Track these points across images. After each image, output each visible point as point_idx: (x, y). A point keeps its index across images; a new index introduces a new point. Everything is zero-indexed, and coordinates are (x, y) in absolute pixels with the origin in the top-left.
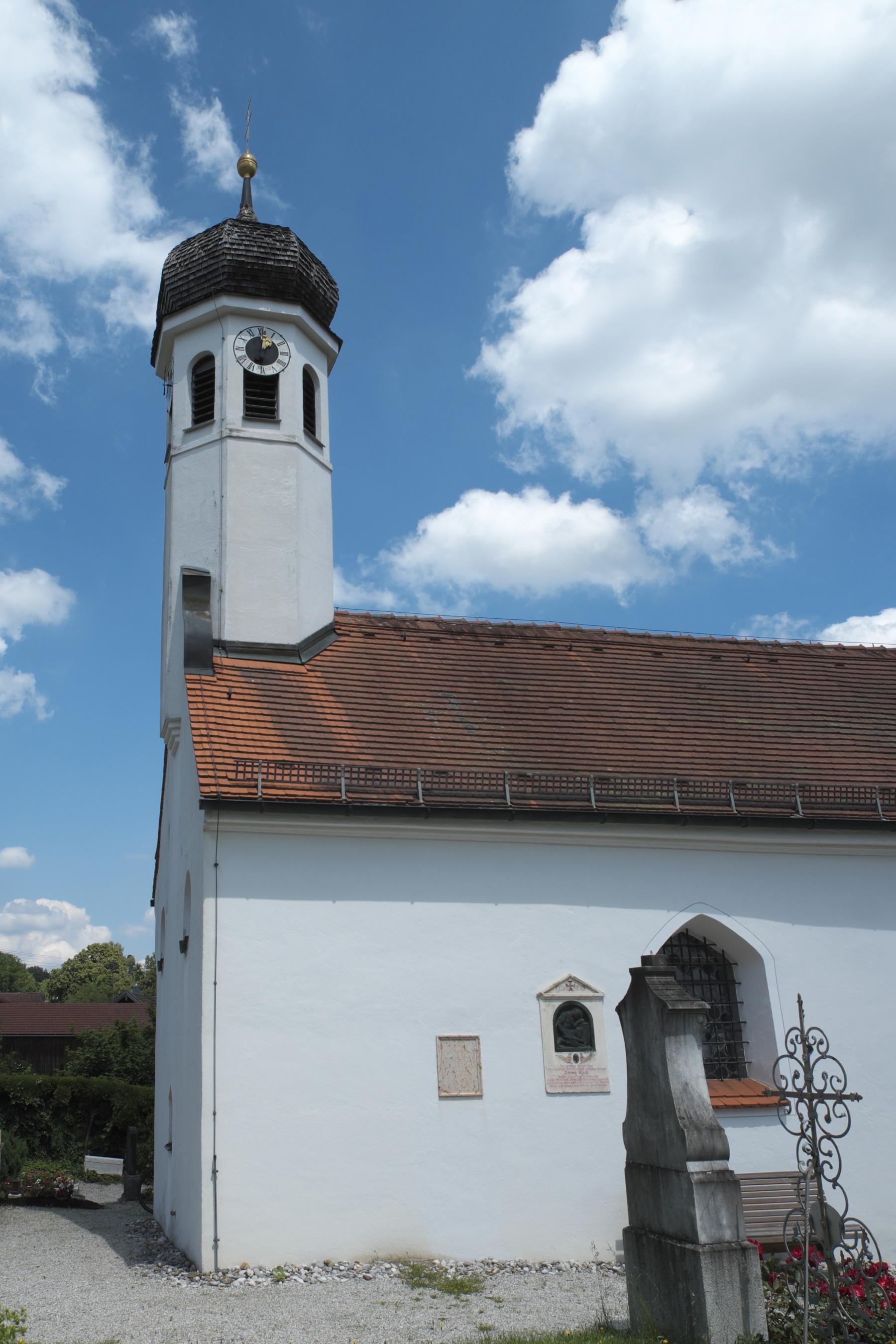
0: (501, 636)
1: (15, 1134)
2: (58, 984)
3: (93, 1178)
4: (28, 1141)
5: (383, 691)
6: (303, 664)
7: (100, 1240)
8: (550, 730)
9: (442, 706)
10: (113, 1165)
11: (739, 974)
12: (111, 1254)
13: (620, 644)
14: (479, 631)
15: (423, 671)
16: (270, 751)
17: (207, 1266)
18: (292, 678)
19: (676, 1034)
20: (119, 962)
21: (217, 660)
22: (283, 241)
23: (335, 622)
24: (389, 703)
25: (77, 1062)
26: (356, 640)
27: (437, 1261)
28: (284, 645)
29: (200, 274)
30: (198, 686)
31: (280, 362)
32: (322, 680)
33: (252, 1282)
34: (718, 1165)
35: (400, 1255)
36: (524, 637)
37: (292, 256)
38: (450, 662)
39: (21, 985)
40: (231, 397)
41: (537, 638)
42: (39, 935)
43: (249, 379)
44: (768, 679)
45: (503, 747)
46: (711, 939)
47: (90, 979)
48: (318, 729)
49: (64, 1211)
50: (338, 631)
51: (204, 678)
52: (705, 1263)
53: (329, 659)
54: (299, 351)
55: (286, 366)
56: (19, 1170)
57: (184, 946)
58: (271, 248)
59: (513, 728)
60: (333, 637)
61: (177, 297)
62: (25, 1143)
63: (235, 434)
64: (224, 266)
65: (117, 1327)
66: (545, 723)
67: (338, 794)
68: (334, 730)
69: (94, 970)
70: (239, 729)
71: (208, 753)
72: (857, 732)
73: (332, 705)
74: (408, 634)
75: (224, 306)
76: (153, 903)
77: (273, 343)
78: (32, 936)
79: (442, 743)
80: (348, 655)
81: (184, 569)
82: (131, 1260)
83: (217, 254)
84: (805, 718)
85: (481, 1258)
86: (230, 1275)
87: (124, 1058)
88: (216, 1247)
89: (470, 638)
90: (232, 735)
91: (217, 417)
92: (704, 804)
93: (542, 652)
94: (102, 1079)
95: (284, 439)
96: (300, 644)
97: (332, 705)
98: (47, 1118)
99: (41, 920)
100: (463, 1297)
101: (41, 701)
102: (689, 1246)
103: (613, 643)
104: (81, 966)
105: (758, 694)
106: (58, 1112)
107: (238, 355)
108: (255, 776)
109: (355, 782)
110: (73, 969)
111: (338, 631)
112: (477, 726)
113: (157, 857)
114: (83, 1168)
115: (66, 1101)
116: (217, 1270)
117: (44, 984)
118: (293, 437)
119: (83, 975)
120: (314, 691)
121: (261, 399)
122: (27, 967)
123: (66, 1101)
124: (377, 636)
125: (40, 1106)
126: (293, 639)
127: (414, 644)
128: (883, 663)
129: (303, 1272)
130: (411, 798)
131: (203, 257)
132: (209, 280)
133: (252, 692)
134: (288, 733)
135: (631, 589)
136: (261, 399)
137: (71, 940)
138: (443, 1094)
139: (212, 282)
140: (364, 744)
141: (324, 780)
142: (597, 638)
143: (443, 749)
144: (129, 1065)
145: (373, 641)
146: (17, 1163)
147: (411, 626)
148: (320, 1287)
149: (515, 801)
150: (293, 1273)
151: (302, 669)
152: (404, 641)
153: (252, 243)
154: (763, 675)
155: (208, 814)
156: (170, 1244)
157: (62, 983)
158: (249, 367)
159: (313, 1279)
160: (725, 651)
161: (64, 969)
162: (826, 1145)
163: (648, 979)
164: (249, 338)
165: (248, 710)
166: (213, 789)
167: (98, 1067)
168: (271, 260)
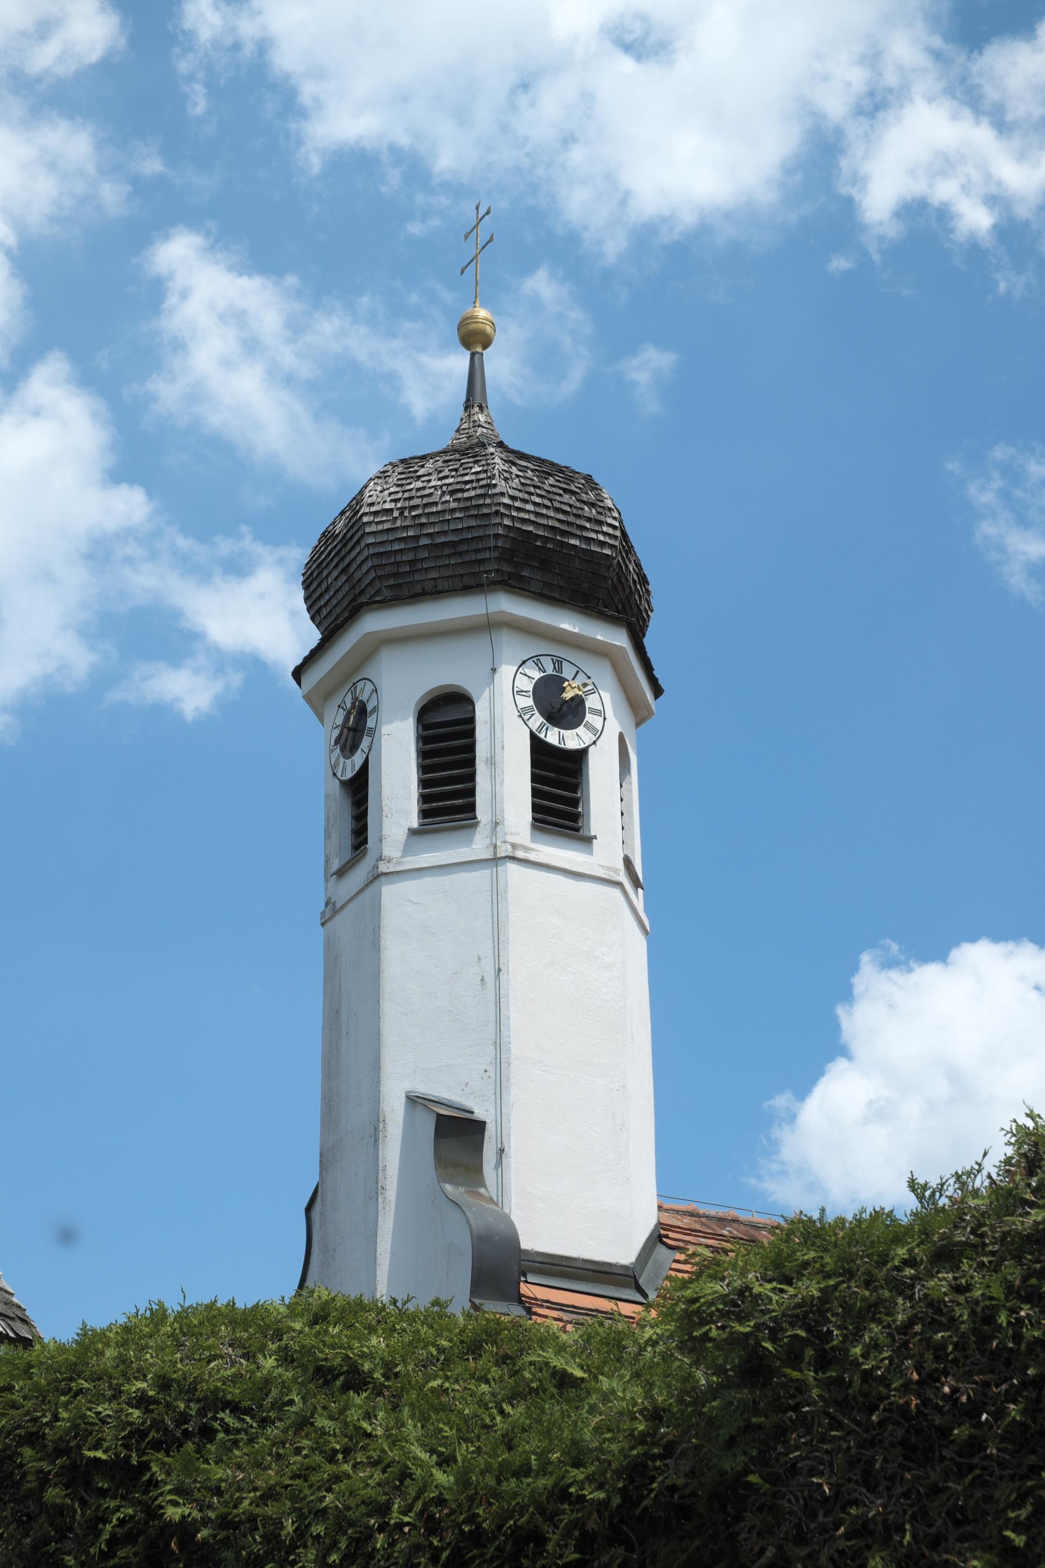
28: (610, 1265)
31: (590, 727)
40: (506, 781)
43: (539, 748)
55: (598, 734)
61: (388, 570)
63: (520, 854)
64: (497, 536)
75: (502, 612)
83: (486, 511)
95: (601, 873)
107: (520, 706)
121: (559, 790)
131: (453, 510)
132: (461, 554)
136: (559, 790)
139: (466, 558)
164: (537, 675)
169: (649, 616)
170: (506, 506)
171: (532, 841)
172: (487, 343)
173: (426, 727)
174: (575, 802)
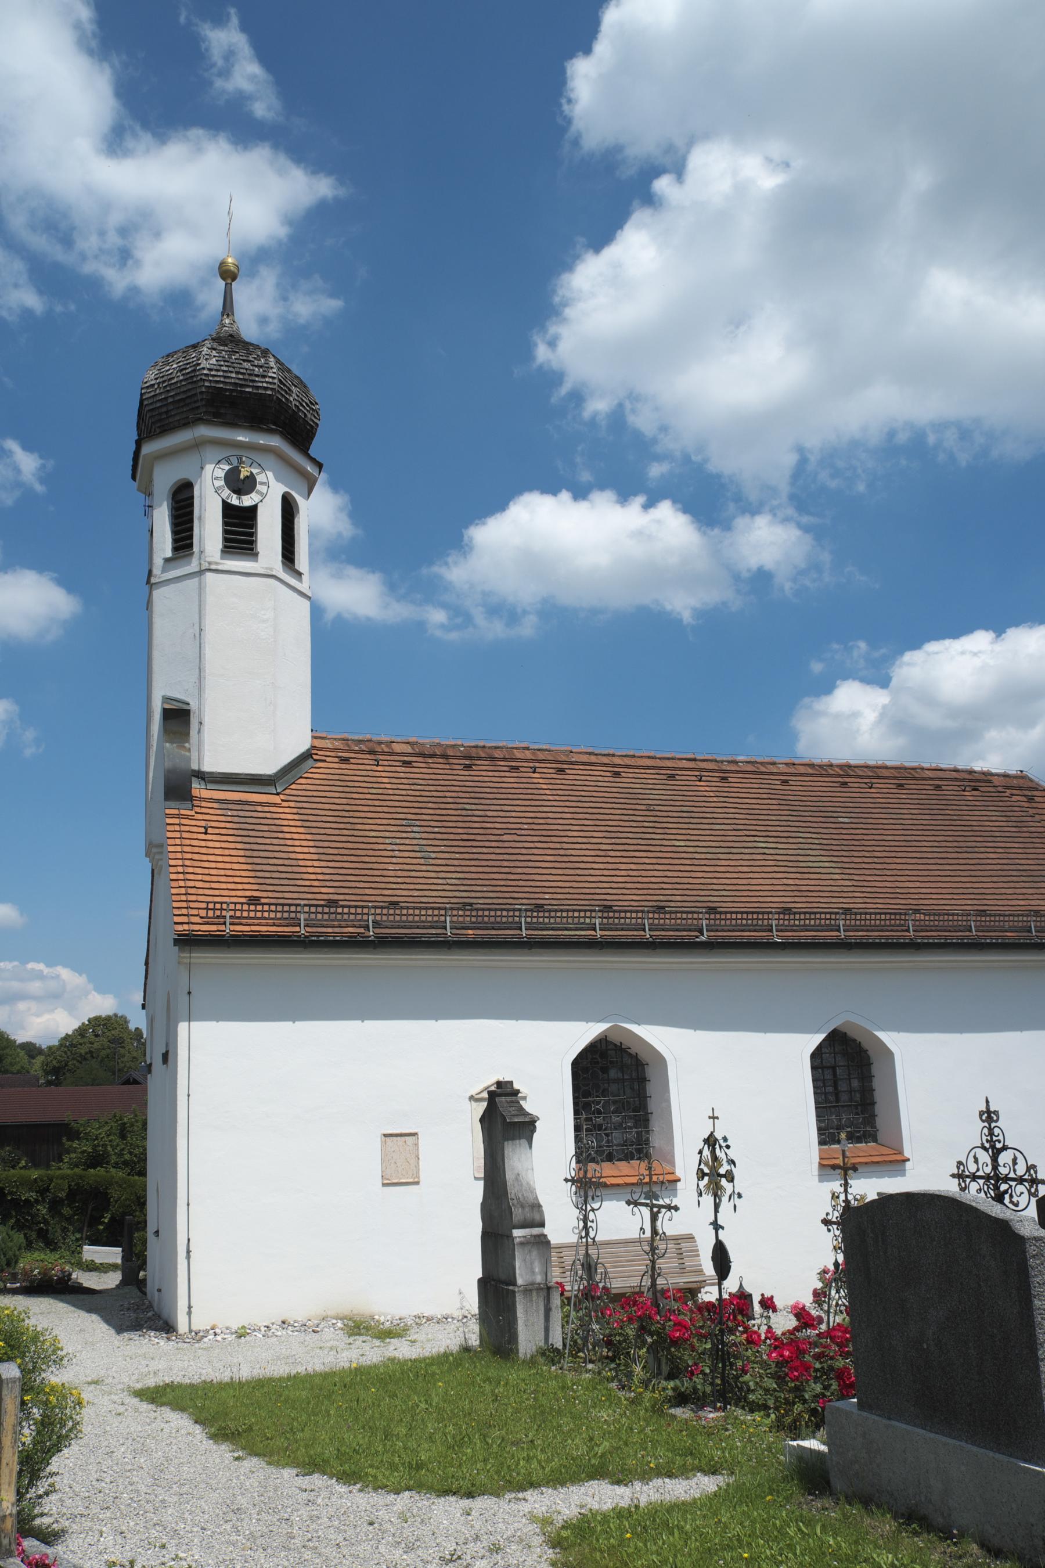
0: (471, 758)
1: (12, 1228)
2: (54, 1062)
3: (92, 1267)
4: (25, 1235)
5: (352, 820)
6: (278, 794)
7: (94, 1317)
8: (501, 857)
9: (404, 835)
10: (113, 1255)
11: (650, 1072)
12: (104, 1327)
13: (583, 764)
14: (450, 753)
15: (392, 797)
16: (240, 887)
17: (182, 1326)
18: (266, 809)
19: (513, 1139)
20: (125, 1036)
21: (195, 792)
22: (261, 367)
23: (313, 747)
24: (356, 833)
25: (73, 1155)
26: (330, 766)
27: (376, 1317)
29: (178, 398)
30: (176, 821)
31: (258, 492)
32: (295, 811)
33: (219, 1338)
34: (536, 1231)
35: (346, 1313)
36: (493, 759)
37: (271, 383)
38: (419, 787)
39: (11, 1064)
40: (210, 528)
41: (504, 759)
42: (33, 1005)
43: (228, 510)
44: (715, 799)
45: (454, 875)
46: (626, 1043)
47: (92, 1057)
48: (287, 862)
49: (63, 1296)
50: (315, 757)
51: (183, 812)
52: (519, 1299)
53: (304, 787)
54: (278, 479)
55: (264, 496)
56: (16, 1262)
57: (165, 1058)
58: (250, 375)
59: (466, 856)
60: (310, 762)
61: (157, 418)
62: (22, 1236)
63: (213, 567)
64: (202, 393)
65: (102, 1373)
66: (497, 851)
67: (297, 929)
68: (301, 863)
69: (96, 1045)
70: (213, 865)
71: (183, 891)
72: (782, 852)
73: (303, 837)
74: (381, 757)
76: (143, 1007)
77: (252, 473)
78: (22, 1006)
79: (399, 873)
80: (322, 782)
81: (166, 699)
82: (120, 1330)
84: (737, 839)
85: (415, 1313)
86: (201, 1334)
87: (123, 1149)
88: (189, 1313)
89: (441, 760)
90: (206, 871)
91: (196, 549)
92: (622, 930)
93: (507, 774)
94: (100, 1171)
96: (277, 773)
97: (303, 837)
98: (44, 1211)
99: (35, 987)
100: (388, 1340)
101: (30, 734)
102: (511, 1288)
103: (577, 763)
104: (81, 1041)
105: (701, 815)
106: (55, 1206)
108: (224, 913)
109: (313, 916)
110: (72, 1045)
111: (315, 757)
112: (433, 855)
113: (147, 964)
114: (81, 1258)
115: (62, 1195)
116: (191, 1331)
117: (39, 1060)
118: (271, 569)
119: (83, 1052)
120: (285, 823)
121: (239, 530)
122: (18, 1042)
123: (62, 1195)
124: (352, 761)
125: (37, 1201)
126: (269, 769)
127: (387, 769)
128: (826, 779)
129: (263, 1329)
130: (362, 930)
133: (228, 825)
134: (259, 867)
135: (700, 614)
136: (239, 530)
137: (71, 1009)
138: (386, 1182)
140: (327, 877)
141: (286, 915)
142: (564, 758)
143: (399, 880)
144: (127, 1157)
145: (348, 766)
146: (15, 1255)
147: (386, 750)
148: (274, 1339)
149: (455, 931)
150: (254, 1330)
151: (277, 799)
152: (377, 765)
153: (231, 369)
154: (712, 794)
155: (181, 950)
156: (158, 1316)
157: (59, 1062)
158: (228, 498)
159: (270, 1334)
160: (681, 769)
161: (61, 1045)
162: (591, 1216)
163: (497, 1099)
164: (227, 467)
165: (223, 845)
166: (186, 927)
167: (96, 1160)
168: (249, 386)
169: (317, 425)
170: (206, 375)
171: (222, 558)
172: (234, 279)
173: (177, 502)
174: (252, 534)
